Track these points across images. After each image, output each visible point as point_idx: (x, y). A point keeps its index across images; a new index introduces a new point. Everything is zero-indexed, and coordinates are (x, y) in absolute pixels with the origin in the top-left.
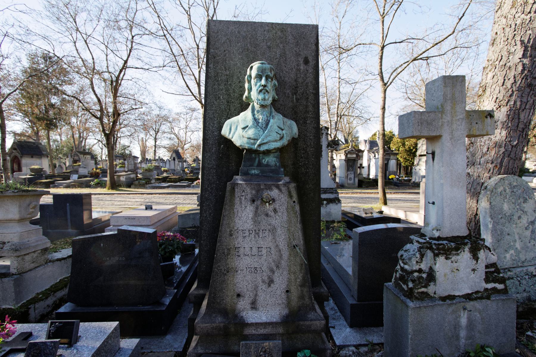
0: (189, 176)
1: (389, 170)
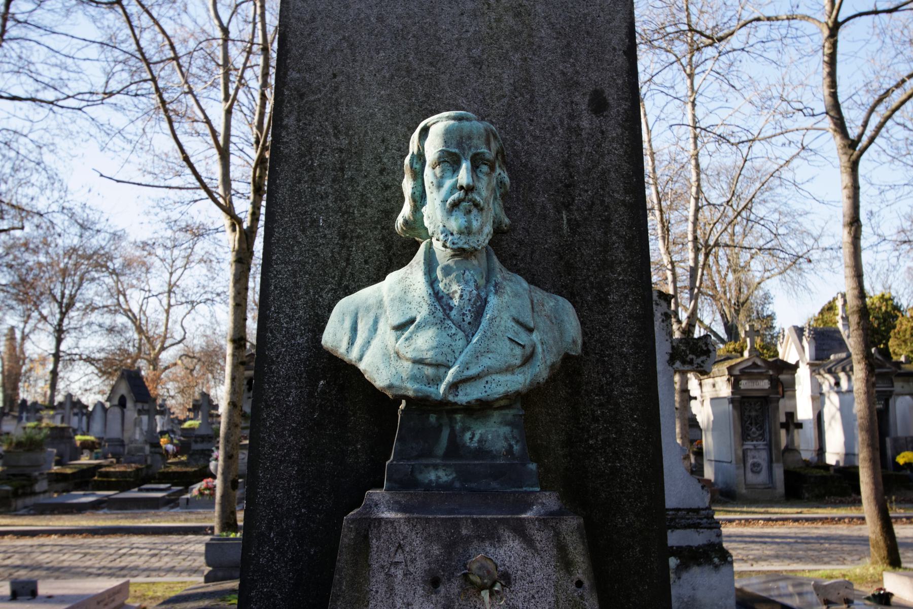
0: (174, 465)
1: (893, 434)
